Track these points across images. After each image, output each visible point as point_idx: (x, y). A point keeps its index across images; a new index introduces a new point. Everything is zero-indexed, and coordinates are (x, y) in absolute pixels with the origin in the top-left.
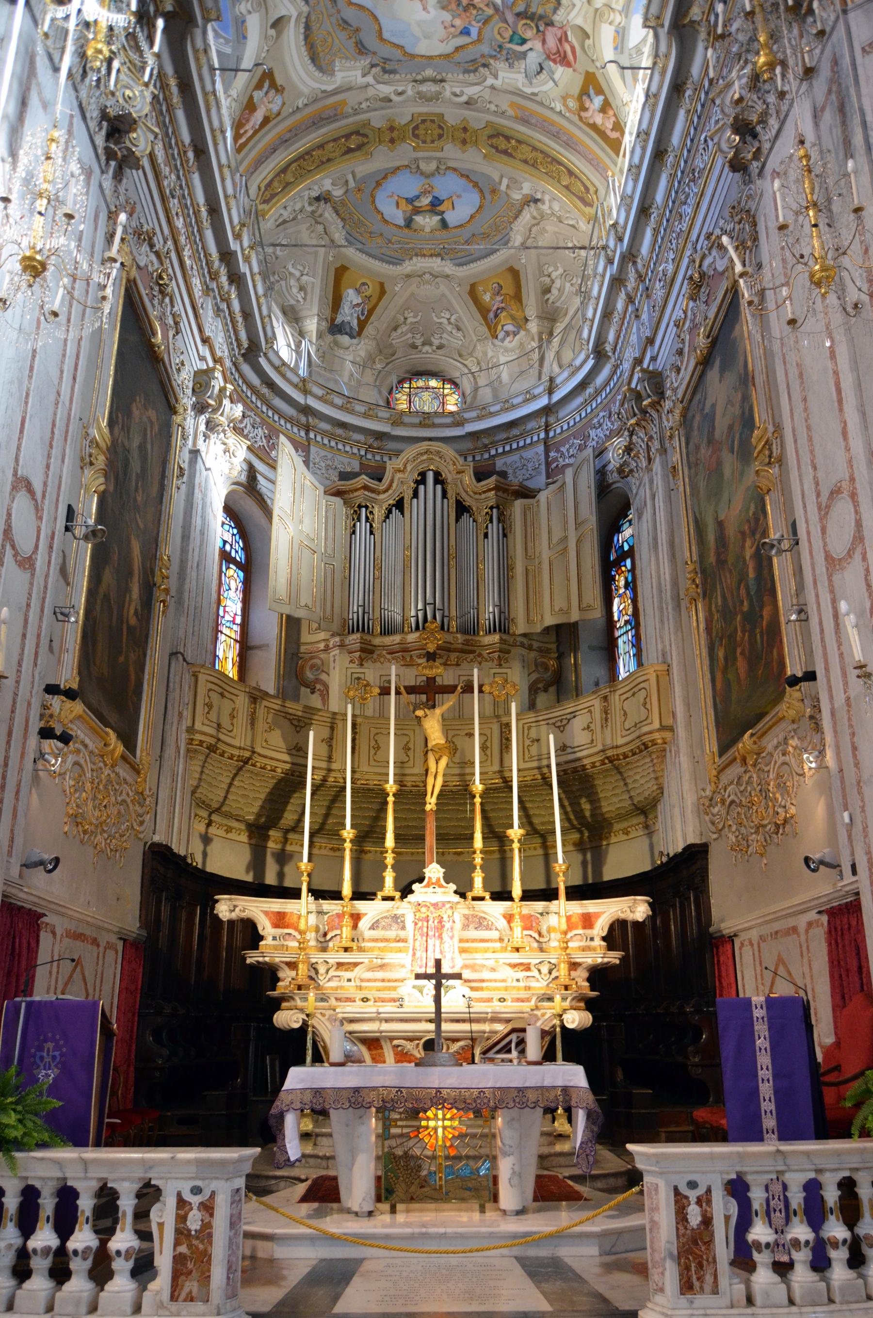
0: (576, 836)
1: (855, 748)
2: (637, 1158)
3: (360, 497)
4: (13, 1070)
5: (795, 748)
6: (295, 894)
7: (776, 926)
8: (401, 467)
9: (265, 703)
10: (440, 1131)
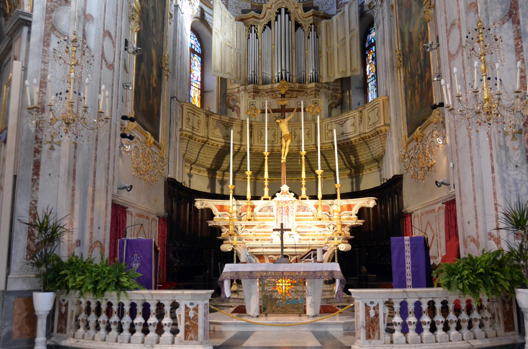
0: (348, 171)
1: (456, 136)
2: (352, 294)
3: (251, 21)
4: (124, 263)
5: (437, 135)
6: (227, 198)
7: (427, 209)
8: (270, 6)
9: (212, 117)
10: (284, 287)
